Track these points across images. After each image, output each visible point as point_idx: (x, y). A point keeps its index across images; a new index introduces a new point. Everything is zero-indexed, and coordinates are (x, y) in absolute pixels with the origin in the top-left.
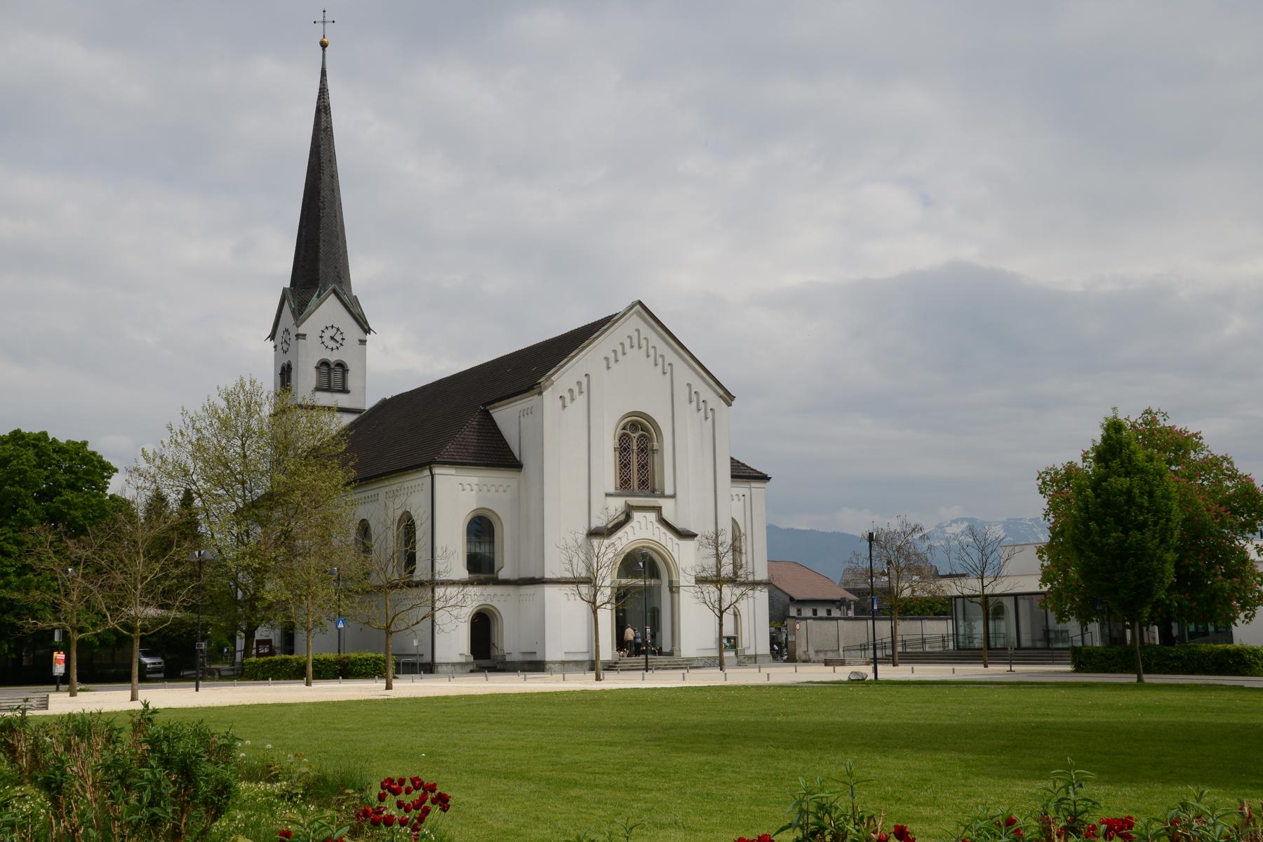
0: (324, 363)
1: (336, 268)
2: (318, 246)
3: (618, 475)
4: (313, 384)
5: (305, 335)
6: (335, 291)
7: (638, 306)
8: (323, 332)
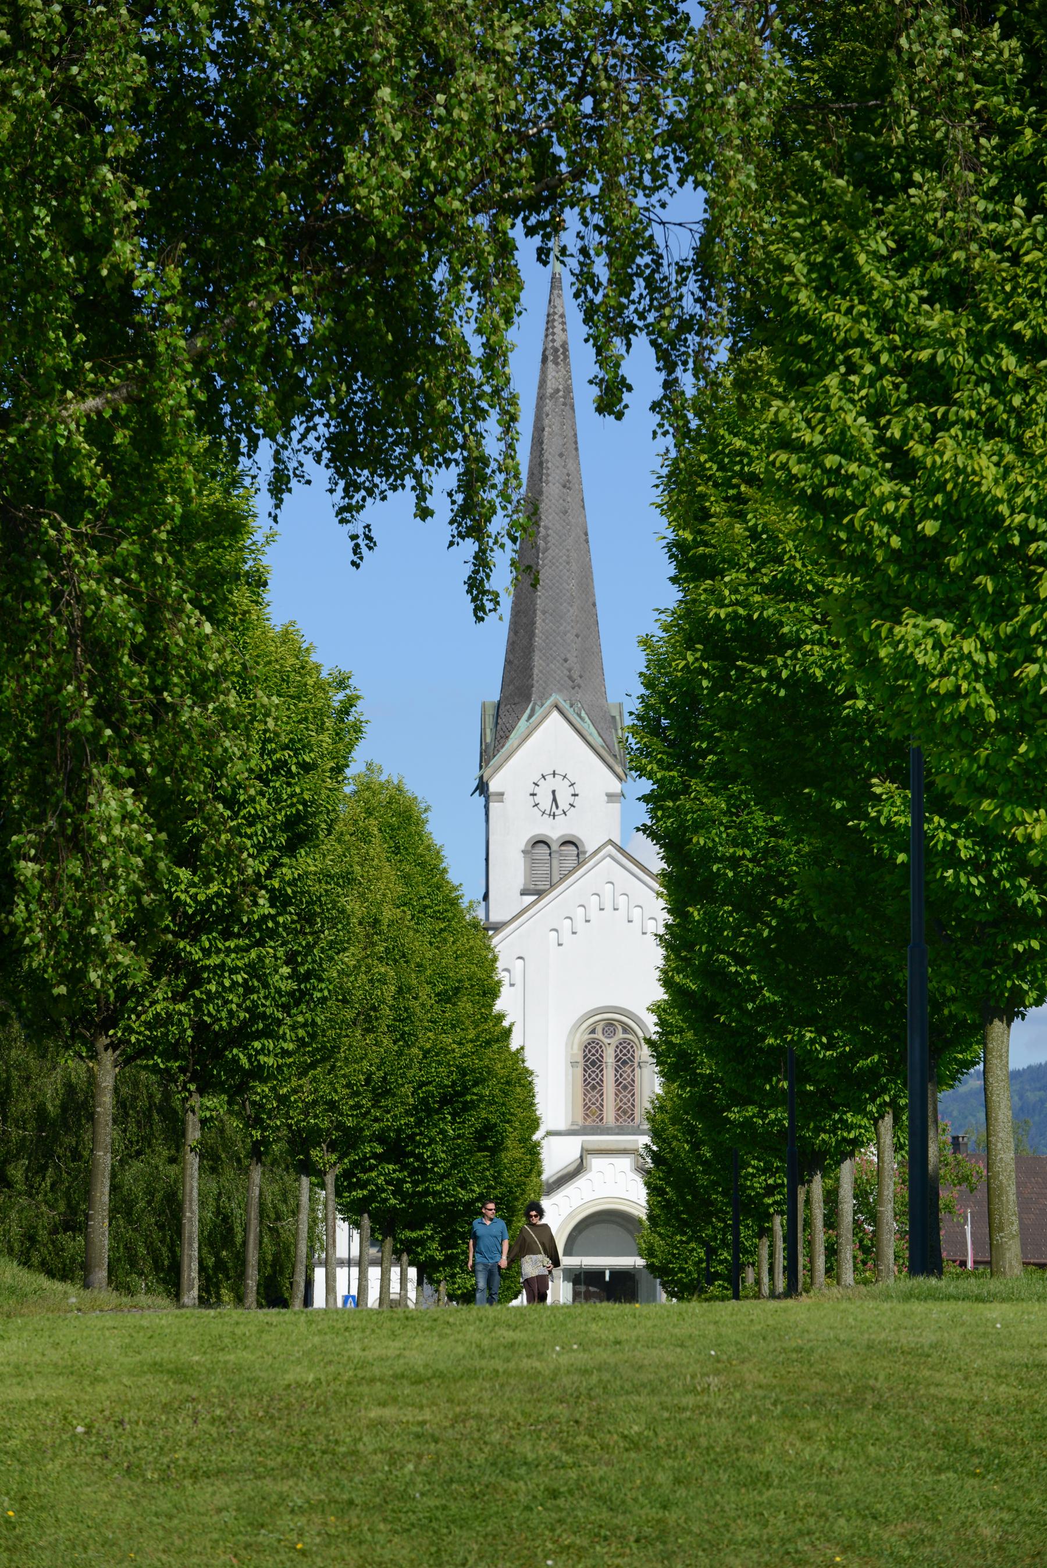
0: (540, 842)
3: (580, 1103)
4: (519, 881)
5: (502, 794)
6: (557, 707)
7: (610, 847)
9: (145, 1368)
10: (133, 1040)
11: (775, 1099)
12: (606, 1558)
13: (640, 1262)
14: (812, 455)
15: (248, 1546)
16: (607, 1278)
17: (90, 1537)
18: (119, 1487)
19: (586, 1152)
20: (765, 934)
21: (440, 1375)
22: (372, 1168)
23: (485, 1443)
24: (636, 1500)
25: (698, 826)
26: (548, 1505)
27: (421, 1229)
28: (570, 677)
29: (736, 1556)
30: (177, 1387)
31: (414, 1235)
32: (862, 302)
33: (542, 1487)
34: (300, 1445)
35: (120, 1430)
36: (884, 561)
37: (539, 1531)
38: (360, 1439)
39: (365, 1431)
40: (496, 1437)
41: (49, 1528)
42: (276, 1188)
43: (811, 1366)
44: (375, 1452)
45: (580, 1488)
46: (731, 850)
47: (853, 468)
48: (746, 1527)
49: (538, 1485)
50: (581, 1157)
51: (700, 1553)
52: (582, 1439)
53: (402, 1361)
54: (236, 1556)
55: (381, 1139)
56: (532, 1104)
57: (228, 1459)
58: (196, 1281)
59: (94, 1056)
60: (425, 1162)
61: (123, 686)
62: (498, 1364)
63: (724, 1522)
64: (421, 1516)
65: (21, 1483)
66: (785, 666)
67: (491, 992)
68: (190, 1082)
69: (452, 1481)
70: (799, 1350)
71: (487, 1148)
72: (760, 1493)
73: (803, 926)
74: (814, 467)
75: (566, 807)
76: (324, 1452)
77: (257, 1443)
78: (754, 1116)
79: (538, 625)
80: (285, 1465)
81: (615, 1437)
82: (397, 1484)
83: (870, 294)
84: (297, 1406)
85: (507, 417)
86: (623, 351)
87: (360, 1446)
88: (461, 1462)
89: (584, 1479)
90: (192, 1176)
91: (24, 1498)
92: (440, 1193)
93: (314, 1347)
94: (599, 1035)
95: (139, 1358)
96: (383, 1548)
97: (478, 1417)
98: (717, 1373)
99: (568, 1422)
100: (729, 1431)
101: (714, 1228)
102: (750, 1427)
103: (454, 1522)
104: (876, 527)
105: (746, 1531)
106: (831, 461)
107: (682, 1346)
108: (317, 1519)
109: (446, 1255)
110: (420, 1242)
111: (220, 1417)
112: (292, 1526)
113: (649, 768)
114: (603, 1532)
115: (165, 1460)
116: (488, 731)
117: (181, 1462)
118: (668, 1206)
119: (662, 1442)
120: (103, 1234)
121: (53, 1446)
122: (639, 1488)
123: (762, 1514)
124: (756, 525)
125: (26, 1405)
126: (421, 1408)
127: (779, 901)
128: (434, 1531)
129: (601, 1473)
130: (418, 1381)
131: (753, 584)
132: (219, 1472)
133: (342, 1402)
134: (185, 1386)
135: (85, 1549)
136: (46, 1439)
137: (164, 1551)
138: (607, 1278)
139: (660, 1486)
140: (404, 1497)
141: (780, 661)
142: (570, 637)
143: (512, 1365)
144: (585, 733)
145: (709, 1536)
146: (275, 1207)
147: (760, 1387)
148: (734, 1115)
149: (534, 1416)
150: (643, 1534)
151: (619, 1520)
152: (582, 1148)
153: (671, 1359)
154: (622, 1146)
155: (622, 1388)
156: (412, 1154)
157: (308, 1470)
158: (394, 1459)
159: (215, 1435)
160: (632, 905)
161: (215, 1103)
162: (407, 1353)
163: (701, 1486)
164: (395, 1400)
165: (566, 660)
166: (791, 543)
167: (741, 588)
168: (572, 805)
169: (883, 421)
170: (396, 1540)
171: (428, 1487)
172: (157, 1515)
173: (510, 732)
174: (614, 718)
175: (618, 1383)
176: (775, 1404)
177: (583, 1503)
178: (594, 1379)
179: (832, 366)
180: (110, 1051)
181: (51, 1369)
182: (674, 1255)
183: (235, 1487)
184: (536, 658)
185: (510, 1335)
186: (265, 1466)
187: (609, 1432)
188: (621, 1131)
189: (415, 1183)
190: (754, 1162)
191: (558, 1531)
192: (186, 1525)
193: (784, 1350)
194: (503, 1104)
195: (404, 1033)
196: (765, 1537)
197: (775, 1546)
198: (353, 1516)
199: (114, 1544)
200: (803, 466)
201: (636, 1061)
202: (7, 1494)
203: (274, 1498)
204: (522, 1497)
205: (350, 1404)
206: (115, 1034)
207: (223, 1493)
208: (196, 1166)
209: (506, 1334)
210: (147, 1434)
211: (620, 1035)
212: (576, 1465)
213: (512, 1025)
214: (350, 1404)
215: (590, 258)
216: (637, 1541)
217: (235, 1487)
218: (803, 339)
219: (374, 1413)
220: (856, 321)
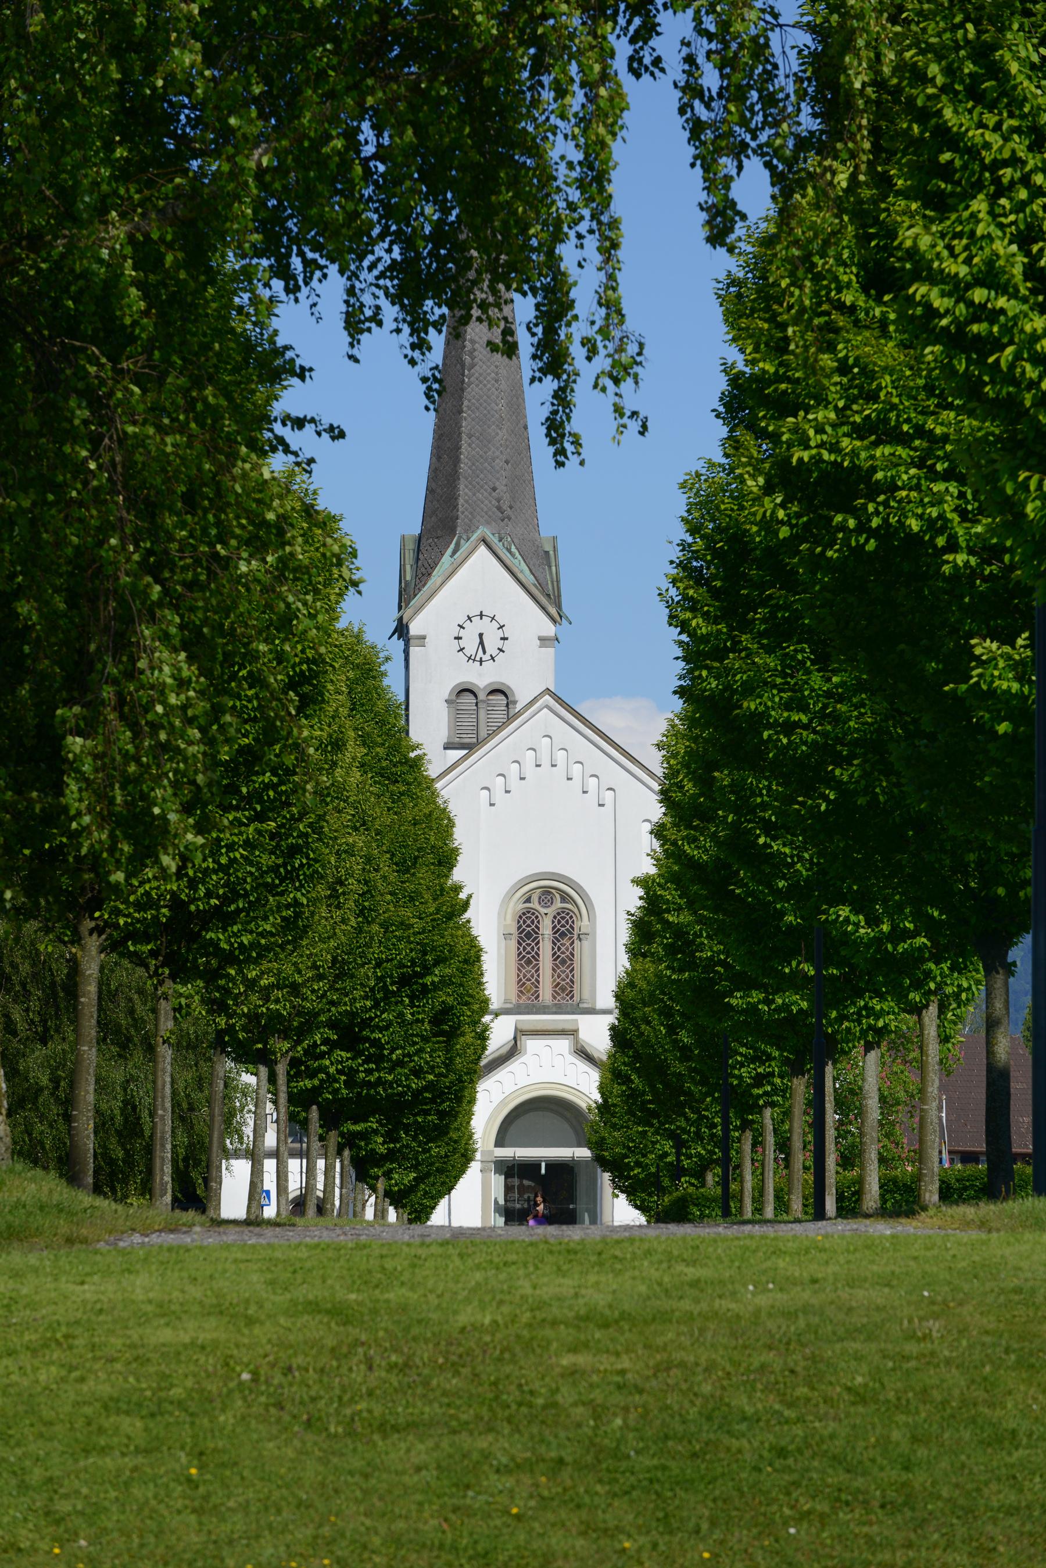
1: (494, 489)
2: (458, 448)
3: (514, 979)
5: (424, 638)
7: (547, 697)
8: (481, 615)
9: (300, 1308)
10: (121, 922)
11: (797, 982)
12: (852, 1526)
13: (584, 1153)
14: (957, 289)
15: (456, 1509)
16: (543, 1171)
17: (283, 1498)
18: (304, 1443)
19: (520, 1033)
20: (823, 808)
21: (625, 1316)
22: (322, 1055)
23: (695, 1394)
24: (873, 1461)
25: (749, 690)
26: (777, 1465)
27: (366, 1121)
28: (499, 508)
29: (995, 1524)
30: (342, 1328)
31: (358, 1128)
32: (1011, 115)
33: (767, 1445)
34: (490, 1395)
35: (290, 1377)
36: (1033, 405)
37: (774, 1494)
38: (558, 1390)
39: (561, 1381)
40: (707, 1388)
41: (236, 1487)
42: (189, 1075)
43: (1037, 1309)
44: (575, 1404)
45: (809, 1446)
46: (786, 714)
47: (1002, 302)
48: (1000, 1492)
49: (762, 1443)
50: (515, 1038)
51: (955, 1521)
52: (802, 1391)
53: (581, 1301)
54: (446, 1520)
55: (332, 1025)
56: (481, 984)
57: (416, 1411)
58: (169, 1186)
59: (77, 939)
60: (382, 1047)
61: (171, 538)
62: (686, 1305)
63: (975, 1485)
64: (641, 1477)
65: (194, 1437)
66: (877, 513)
67: (447, 859)
68: (162, 966)
69: (667, 1437)
70: (1018, 1290)
71: (442, 1033)
72: (1010, 1454)
73: (861, 801)
74: (957, 302)
75: (494, 653)
76: (520, 1404)
77: (445, 1393)
78: (759, 1002)
79: (463, 450)
80: (479, 1418)
81: (838, 1389)
82: (606, 1441)
83: (1021, 106)
84: (478, 1351)
85: (608, 244)
86: (734, 172)
87: (559, 1398)
88: (672, 1417)
89: (813, 1436)
90: (164, 1070)
91: (201, 1454)
92: (391, 1083)
93: (478, 1284)
94: (535, 904)
95: (288, 1296)
96: (604, 1512)
97: (682, 1365)
98: (936, 1317)
99: (782, 1371)
100: (963, 1383)
101: (687, 1119)
102: (985, 1379)
103: (678, 1483)
104: (1028, 367)
105: (1001, 1496)
106: (979, 295)
107: (888, 1285)
108: (527, 1480)
109: (388, 1149)
110: (364, 1135)
111: (396, 1364)
112: (500, 1487)
113: (694, 623)
114: (843, 1497)
115: (348, 1412)
116: (408, 567)
117: (365, 1414)
118: (632, 1095)
119: (891, 1396)
120: (88, 1137)
121: (220, 1395)
122: (874, 1447)
123: (1014, 1477)
124: (847, 357)
125: (181, 1349)
126: (617, 1354)
127: (838, 772)
128: (657, 1493)
129: (830, 1429)
130: (605, 1325)
131: (843, 424)
132: (411, 1426)
133: (528, 1346)
134: (350, 1328)
135: (279, 1511)
136: (212, 1387)
137: (366, 1515)
138: (543, 1171)
139: (898, 1444)
140: (617, 1454)
141: (871, 508)
142: (499, 463)
143: (704, 1306)
144: (515, 570)
145: (961, 1501)
146: (188, 1096)
147: (987, 1332)
148: (736, 1000)
149: (744, 1365)
150: (888, 1499)
151: (859, 1482)
152: (516, 1029)
153: (880, 1301)
154: (560, 1027)
155: (834, 1333)
156: (367, 1039)
157: (505, 1423)
158: (598, 1412)
159: (396, 1384)
160: (571, 762)
161: (190, 990)
162: (583, 1291)
163: (942, 1445)
164: (586, 1345)
165: (494, 489)
166: (888, 378)
167: (828, 429)
168: (501, 650)
169: (1035, 248)
170: (616, 1503)
171: (641, 1445)
172: (351, 1473)
173: (433, 568)
174: (547, 553)
175: (829, 1328)
176: (1007, 1351)
177: (816, 1464)
178: (802, 1323)
179: (978, 186)
180: (95, 936)
181: (196, 1308)
182: (629, 1148)
183: (430, 1443)
184: (462, 487)
185: (692, 1273)
186: (458, 1419)
187: (831, 1383)
188: (559, 1010)
189: (369, 1072)
190: (743, 1050)
191: (794, 1495)
192: (385, 1486)
193: (1002, 1291)
194: (461, 985)
195: (364, 907)
196: (1024, 1504)
197: (1036, 1514)
198: (565, 1474)
199: (307, 1507)
200: (946, 300)
201: (576, 932)
202: (182, 1448)
203: (475, 1456)
204: (748, 1456)
205: (538, 1351)
206: (102, 916)
207: (421, 1451)
208: (168, 1060)
209: (686, 1270)
210: (321, 1381)
211: (558, 904)
212: (802, 1419)
213: (470, 896)
214: (538, 1351)
215: (698, 68)
216: (883, 1506)
217: (430, 1443)
218: (946, 157)
219: (565, 1361)
220: (1006, 139)
